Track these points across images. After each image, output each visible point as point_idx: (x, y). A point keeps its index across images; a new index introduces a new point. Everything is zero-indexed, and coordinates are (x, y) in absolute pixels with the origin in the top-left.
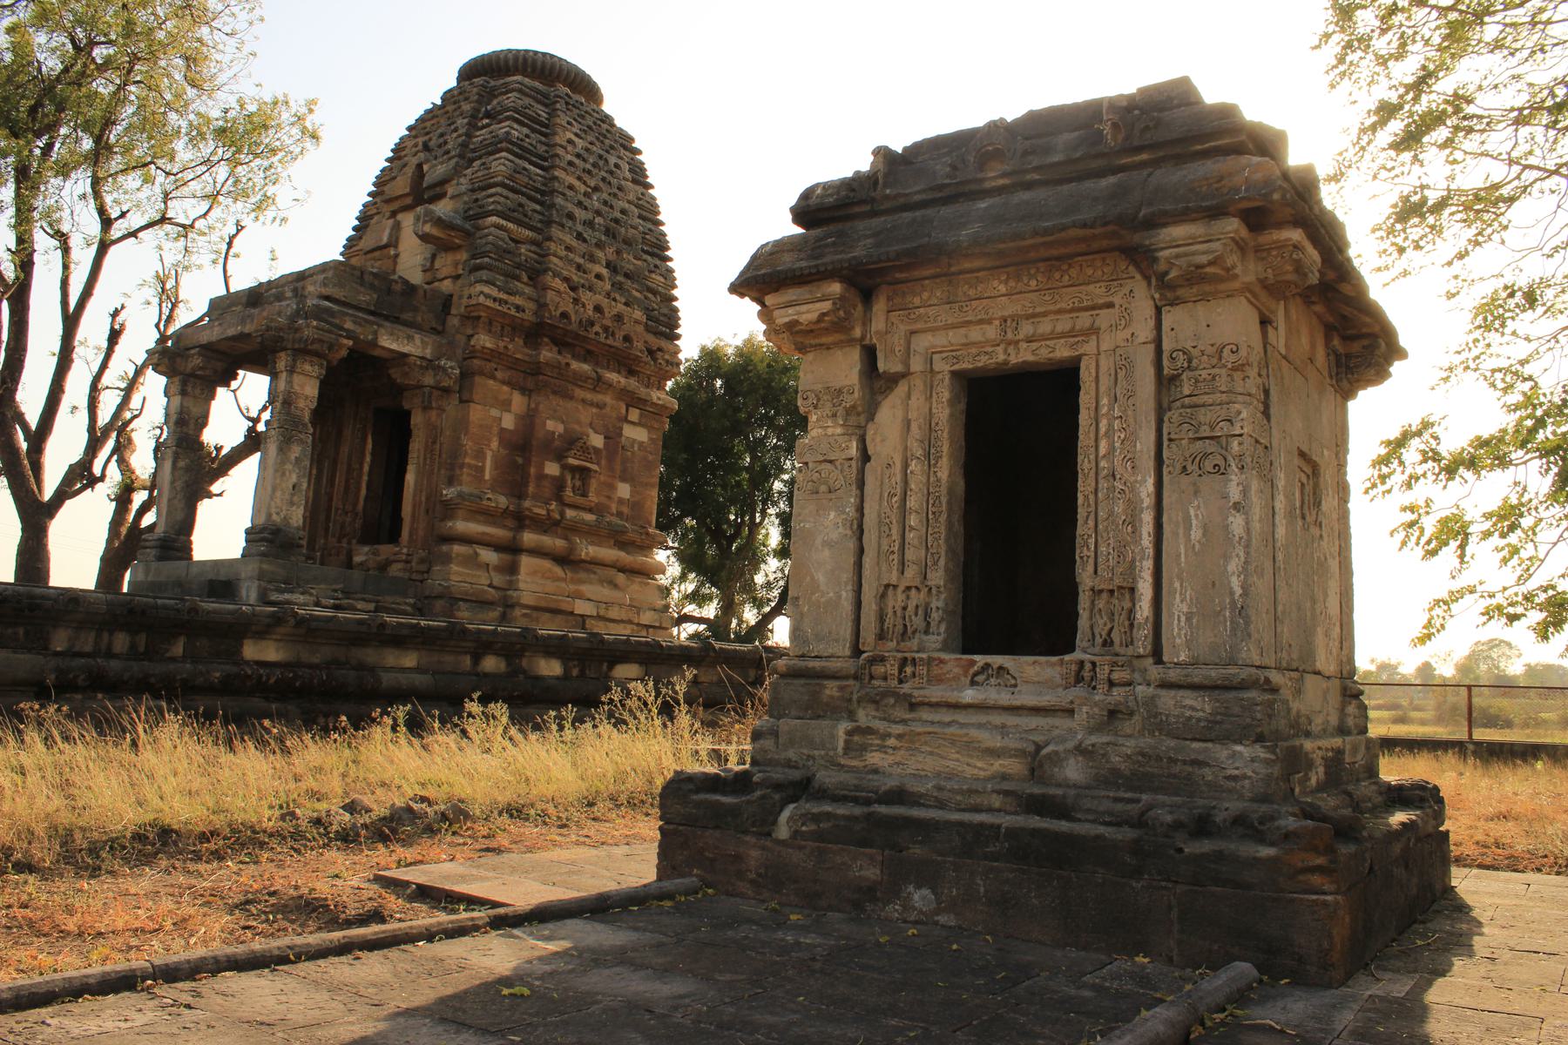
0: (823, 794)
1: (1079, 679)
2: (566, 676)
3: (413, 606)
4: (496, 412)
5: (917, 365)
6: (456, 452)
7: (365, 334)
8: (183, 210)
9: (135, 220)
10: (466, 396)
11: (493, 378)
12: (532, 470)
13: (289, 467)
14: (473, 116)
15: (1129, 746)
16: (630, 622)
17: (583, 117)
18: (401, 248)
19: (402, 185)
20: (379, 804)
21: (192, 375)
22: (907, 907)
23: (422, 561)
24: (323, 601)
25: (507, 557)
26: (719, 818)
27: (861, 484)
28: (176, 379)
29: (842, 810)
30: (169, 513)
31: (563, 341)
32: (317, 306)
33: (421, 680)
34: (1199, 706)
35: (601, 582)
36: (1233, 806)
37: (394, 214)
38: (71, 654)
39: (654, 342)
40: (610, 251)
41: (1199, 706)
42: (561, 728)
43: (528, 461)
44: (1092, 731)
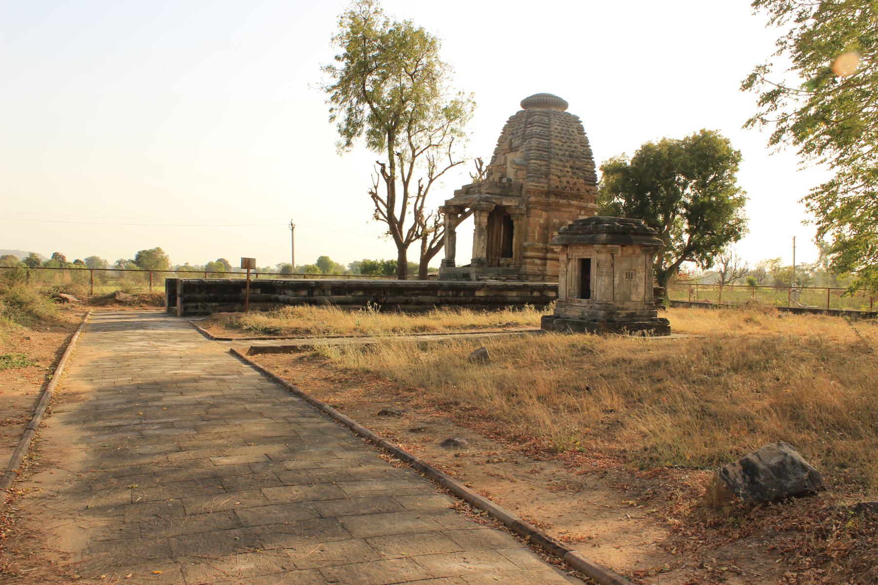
4: (539, 218)
6: (527, 232)
7: (498, 202)
8: (435, 141)
9: (423, 147)
19: (506, 146)
25: (543, 261)
33: (517, 299)
34: (598, 306)
39: (588, 188)
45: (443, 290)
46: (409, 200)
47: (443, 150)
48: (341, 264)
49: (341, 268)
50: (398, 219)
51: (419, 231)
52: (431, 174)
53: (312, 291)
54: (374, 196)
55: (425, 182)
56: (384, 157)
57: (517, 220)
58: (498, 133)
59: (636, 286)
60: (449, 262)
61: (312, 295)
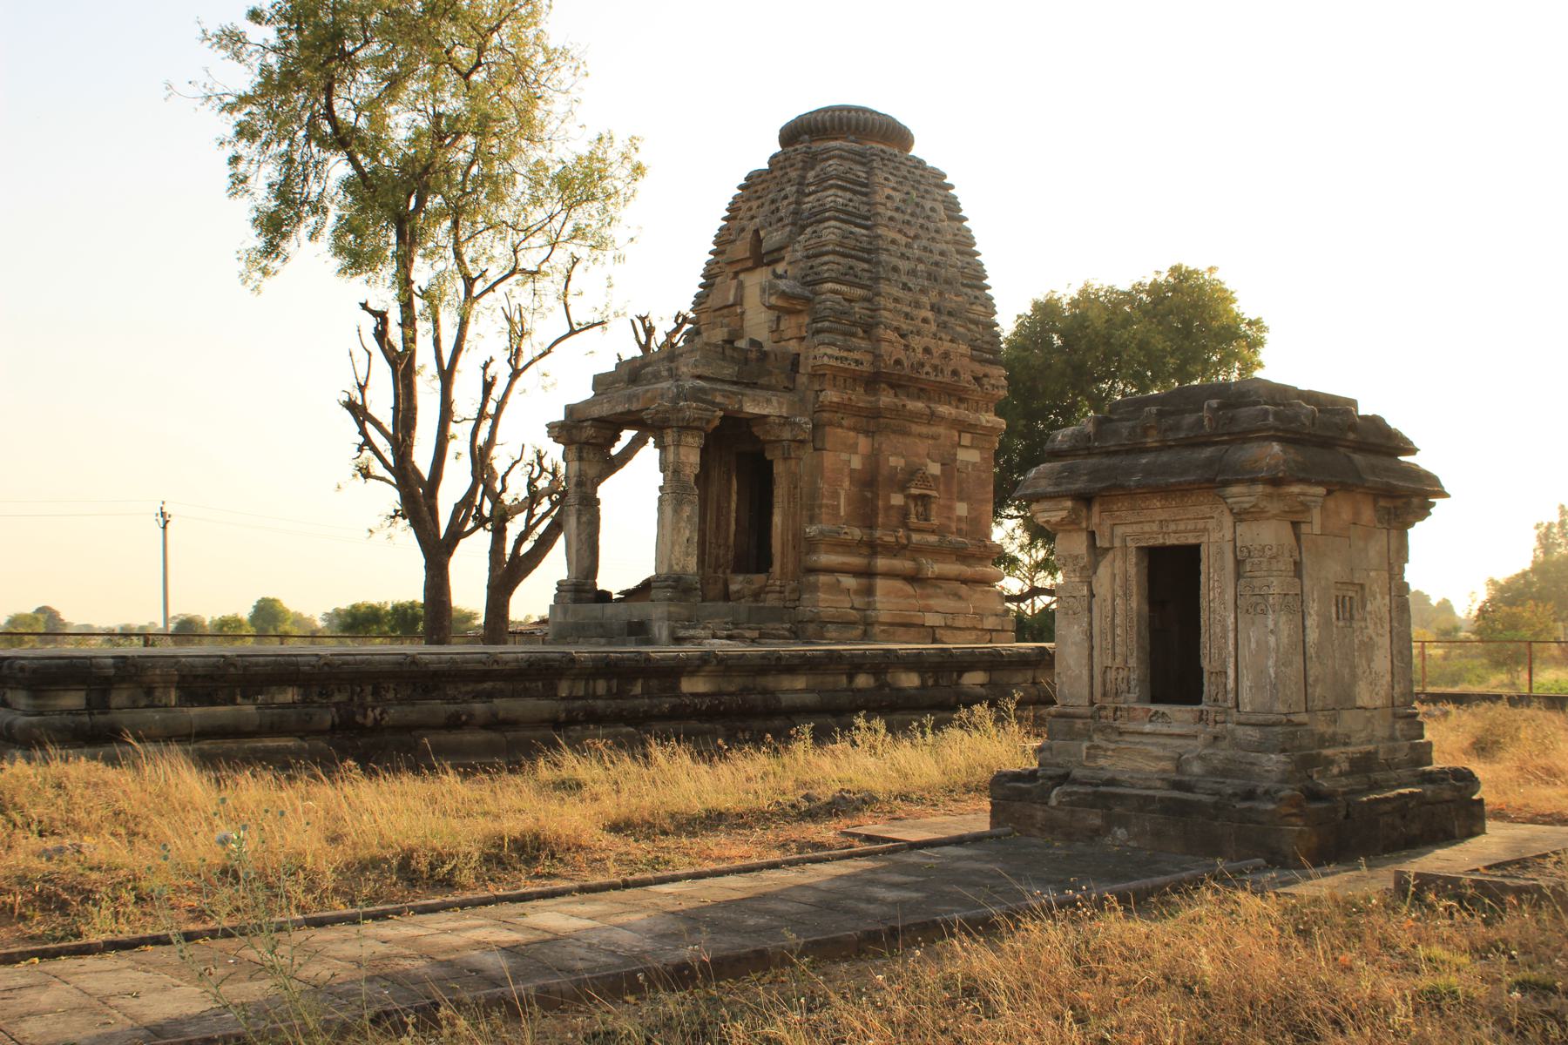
0: (1075, 782)
1: (1201, 719)
2: (923, 686)
3: (789, 630)
4: (846, 455)
5: (1117, 543)
6: (814, 494)
8: (528, 261)
9: (494, 274)
10: (819, 445)
11: (841, 426)
12: (880, 503)
13: (683, 524)
14: (800, 184)
15: (1222, 755)
16: (975, 628)
17: (897, 169)
18: (746, 306)
19: (741, 249)
20: (825, 794)
21: (587, 443)
22: (1114, 838)
23: (793, 591)
24: (719, 633)
25: (864, 581)
26: (1021, 795)
27: (1090, 610)
28: (574, 447)
29: (1082, 789)
30: (578, 561)
31: (897, 385)
32: (693, 388)
33: (810, 699)
34: (1254, 734)
35: (946, 595)
36: (1266, 785)
37: (736, 274)
38: (571, 698)
39: (980, 369)
40: (933, 294)
41: (1254, 734)
42: (924, 734)
43: (876, 496)
44: (1206, 747)
45: (577, 677)
46: (453, 428)
47: (550, 286)
48: (306, 615)
49: (309, 621)
50: (425, 472)
51: (486, 507)
52: (517, 353)
53: (105, 693)
54: (358, 411)
55: (501, 370)
56: (385, 297)
57: (786, 459)
58: (714, 218)
59: (1368, 646)
60: (580, 589)
61: (105, 708)
